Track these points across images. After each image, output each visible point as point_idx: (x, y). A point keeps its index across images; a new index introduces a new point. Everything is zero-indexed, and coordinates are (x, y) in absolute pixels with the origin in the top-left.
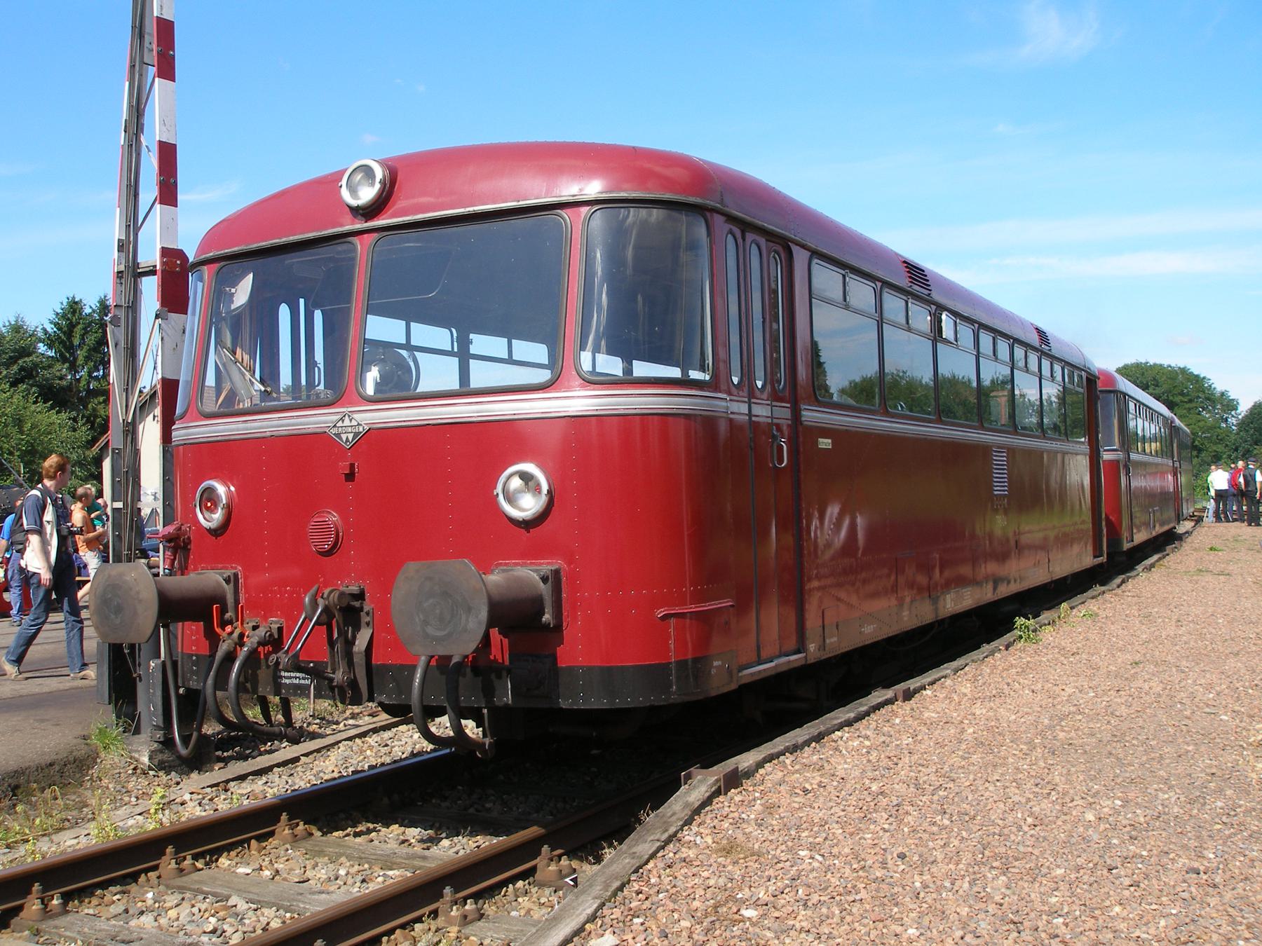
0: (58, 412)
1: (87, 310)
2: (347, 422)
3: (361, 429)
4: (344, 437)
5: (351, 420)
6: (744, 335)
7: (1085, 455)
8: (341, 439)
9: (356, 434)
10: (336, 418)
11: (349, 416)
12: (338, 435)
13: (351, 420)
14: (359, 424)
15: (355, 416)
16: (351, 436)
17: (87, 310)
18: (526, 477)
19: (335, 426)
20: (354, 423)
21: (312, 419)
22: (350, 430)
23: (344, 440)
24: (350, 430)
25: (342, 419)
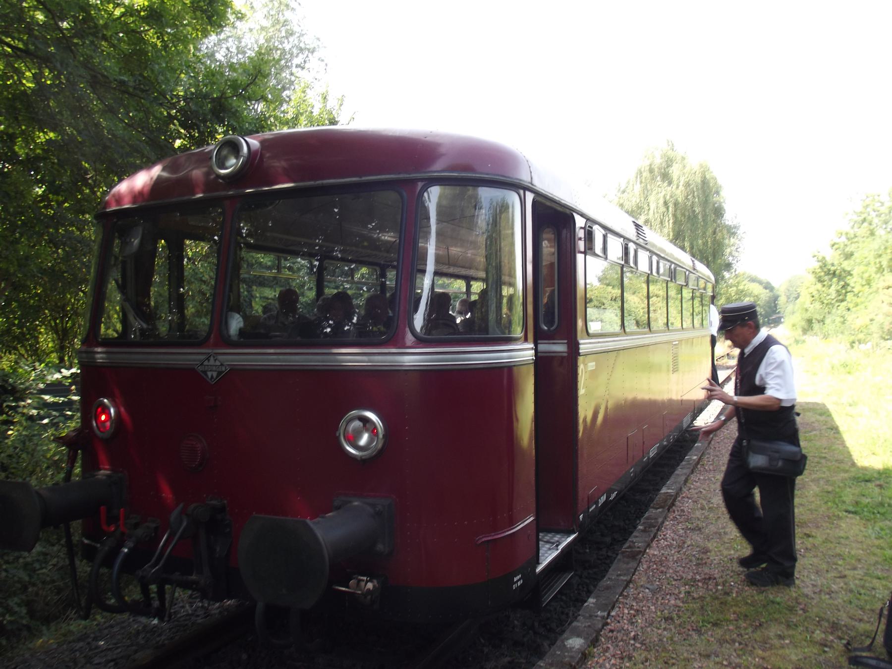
0: (734, 238)
1: (371, 589)
2: (212, 362)
3: (224, 369)
4: (209, 374)
5: (215, 360)
6: (573, 236)
7: (601, 330)
8: (206, 375)
9: (219, 373)
10: (202, 357)
11: (214, 357)
12: (205, 372)
13: (215, 360)
14: (222, 365)
15: (220, 357)
16: (215, 374)
17: (371, 589)
18: (365, 421)
19: (202, 364)
20: (218, 363)
21: (189, 357)
22: (214, 368)
23: (210, 377)
24: (214, 368)
25: (208, 359)
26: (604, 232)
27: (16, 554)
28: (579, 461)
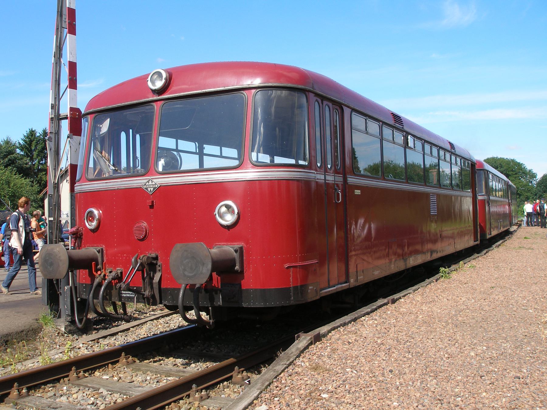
1: (38, 135)
2: (150, 183)
3: (156, 186)
4: (149, 189)
5: (152, 182)
8: (148, 190)
9: (154, 188)
10: (146, 181)
11: (151, 180)
12: (147, 189)
13: (152, 182)
14: (155, 184)
15: (154, 180)
16: (152, 189)
17: (38, 135)
18: (228, 207)
19: (145, 185)
20: (153, 183)
21: (135, 182)
22: (152, 186)
23: (149, 190)
24: (152, 186)
25: (148, 182)
26: (21, 363)
27: (161, 358)
28: (381, 277)
